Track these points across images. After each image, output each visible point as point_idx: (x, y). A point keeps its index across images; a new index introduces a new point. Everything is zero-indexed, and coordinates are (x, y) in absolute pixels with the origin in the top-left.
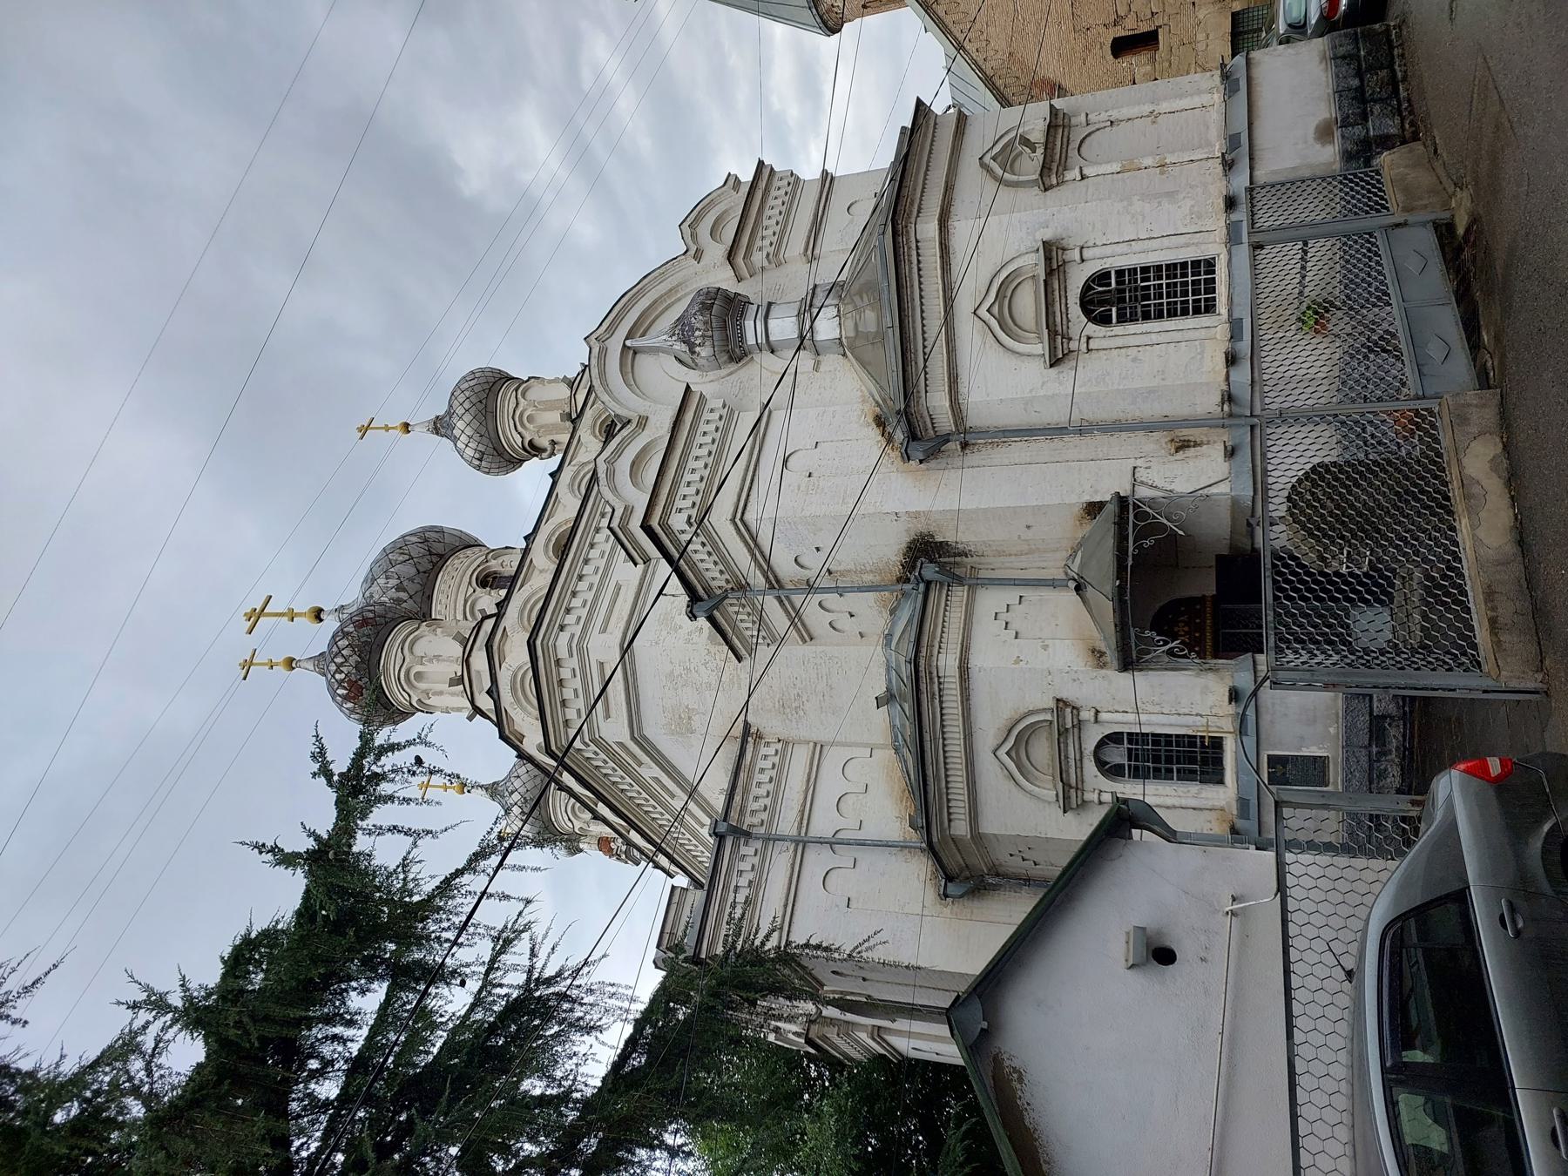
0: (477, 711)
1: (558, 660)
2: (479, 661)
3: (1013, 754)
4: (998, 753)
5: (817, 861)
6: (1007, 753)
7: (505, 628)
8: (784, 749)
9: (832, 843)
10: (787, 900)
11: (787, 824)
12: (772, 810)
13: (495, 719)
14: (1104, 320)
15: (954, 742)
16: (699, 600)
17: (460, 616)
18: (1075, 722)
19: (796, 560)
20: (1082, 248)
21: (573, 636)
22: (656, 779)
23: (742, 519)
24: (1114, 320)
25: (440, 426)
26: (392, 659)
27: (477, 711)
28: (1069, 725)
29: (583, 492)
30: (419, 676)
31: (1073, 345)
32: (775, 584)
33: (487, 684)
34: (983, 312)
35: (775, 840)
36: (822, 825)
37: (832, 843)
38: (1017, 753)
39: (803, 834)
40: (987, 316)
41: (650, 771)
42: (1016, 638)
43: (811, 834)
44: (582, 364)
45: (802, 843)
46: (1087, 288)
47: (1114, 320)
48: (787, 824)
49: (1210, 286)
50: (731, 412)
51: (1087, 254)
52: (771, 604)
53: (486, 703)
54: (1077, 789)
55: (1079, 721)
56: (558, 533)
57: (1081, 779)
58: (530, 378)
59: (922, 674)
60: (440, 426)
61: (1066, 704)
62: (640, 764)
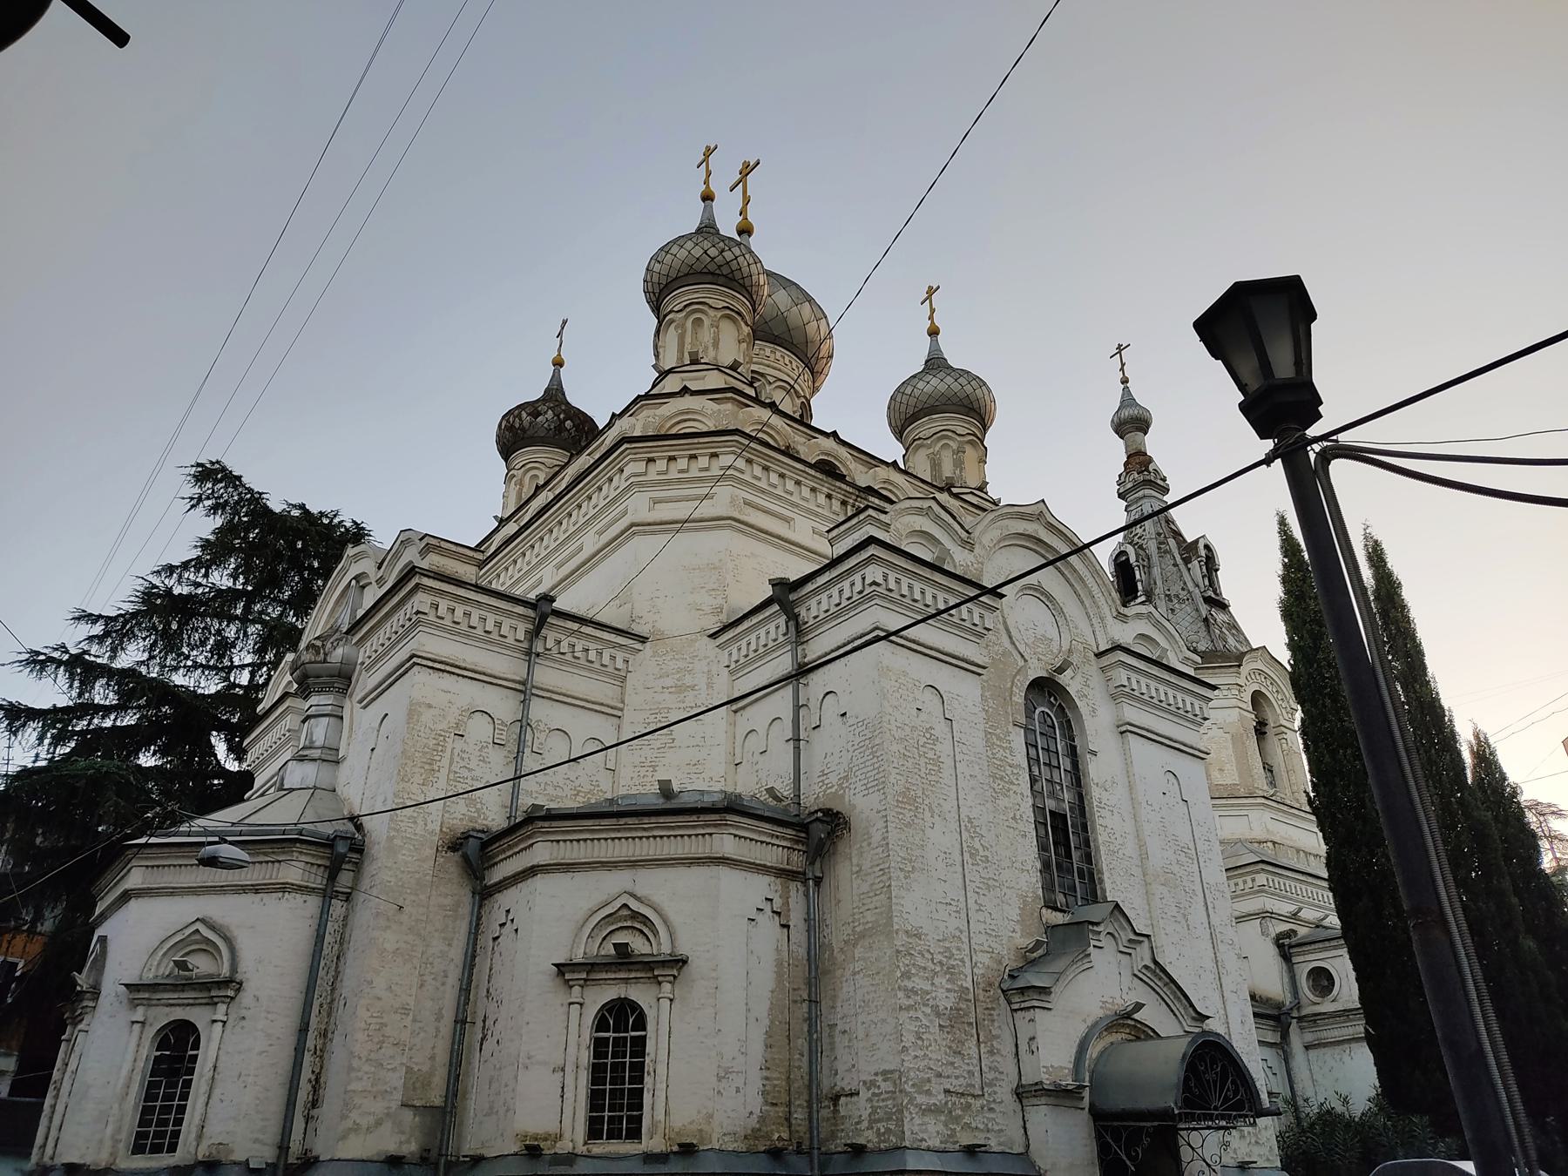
0: (663, 374)
1: (696, 458)
2: (715, 380)
3: (197, 937)
4: (198, 923)
5: (504, 706)
6: (197, 930)
7: (749, 406)
8: (615, 677)
9: (524, 723)
10: (931, 649)
11: (545, 675)
12: (561, 660)
13: (652, 393)
14: (601, 1024)
15: (274, 874)
16: (785, 594)
17: (754, 367)
18: (216, 1000)
19: (831, 692)
20: (581, 1005)
21: (742, 472)
22: (581, 549)
23: (415, 664)
24: (643, 1033)
25: (936, 363)
26: (717, 297)
27: (663, 374)
28: (213, 993)
29: (673, 431)
30: (698, 322)
31: (577, 989)
32: (802, 671)
33: (693, 386)
34: (199, 926)
35: (529, 661)
36: (540, 711)
37: (524, 723)
38: (197, 942)
39: (534, 691)
40: (618, 904)
41: (590, 542)
42: (758, 909)
43: (535, 701)
44: (495, 517)
45: (525, 690)
46: (634, 1006)
47: (643, 1033)
48: (545, 675)
49: (614, 1135)
50: (981, 636)
51: (575, 1008)
52: (783, 664)
53: (672, 384)
54: (585, 980)
55: (216, 1004)
56: (837, 463)
57: (159, 1003)
58: (986, 448)
59: (622, 821)
60: (936, 363)
61: (238, 990)
62: (600, 533)
